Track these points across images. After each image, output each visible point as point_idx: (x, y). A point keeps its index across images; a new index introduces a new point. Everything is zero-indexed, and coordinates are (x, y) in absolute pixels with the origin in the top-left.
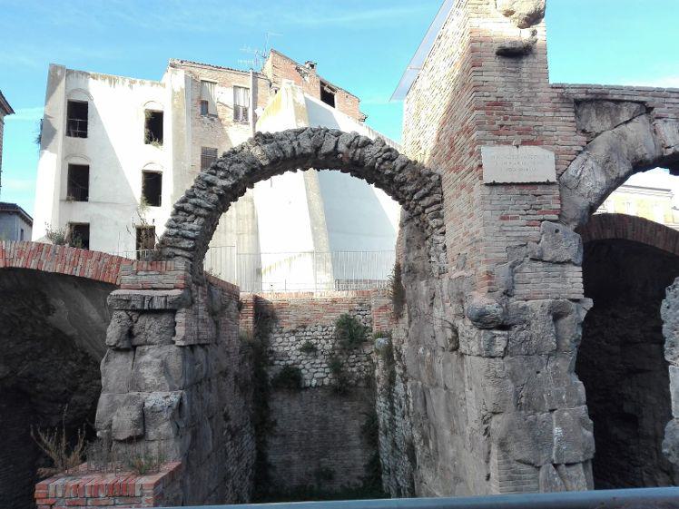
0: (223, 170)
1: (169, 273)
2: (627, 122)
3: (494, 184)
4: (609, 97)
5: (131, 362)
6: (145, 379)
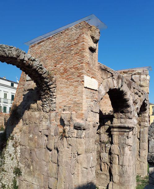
2: (109, 78)
3: (86, 88)
4: (107, 70)
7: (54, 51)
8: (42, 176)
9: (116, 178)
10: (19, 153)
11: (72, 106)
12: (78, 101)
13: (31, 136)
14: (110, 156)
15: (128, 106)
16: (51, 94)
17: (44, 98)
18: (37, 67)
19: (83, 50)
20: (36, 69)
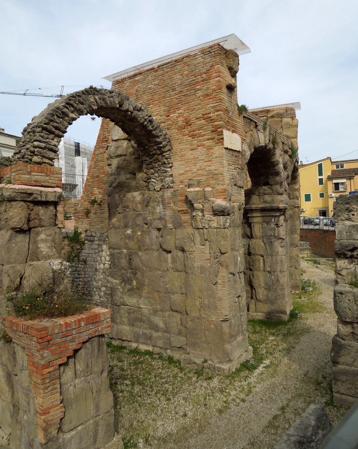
0: (73, 106)
1: (52, 175)
3: (226, 149)
5: (27, 240)
6: (42, 252)
7: (164, 91)
8: (156, 293)
9: (261, 293)
10: (108, 262)
11: (204, 178)
12: (215, 170)
13: (129, 232)
14: (248, 257)
15: (278, 174)
16: (165, 160)
17: (151, 169)
18: (145, 120)
19: (219, 91)
20: (143, 124)
